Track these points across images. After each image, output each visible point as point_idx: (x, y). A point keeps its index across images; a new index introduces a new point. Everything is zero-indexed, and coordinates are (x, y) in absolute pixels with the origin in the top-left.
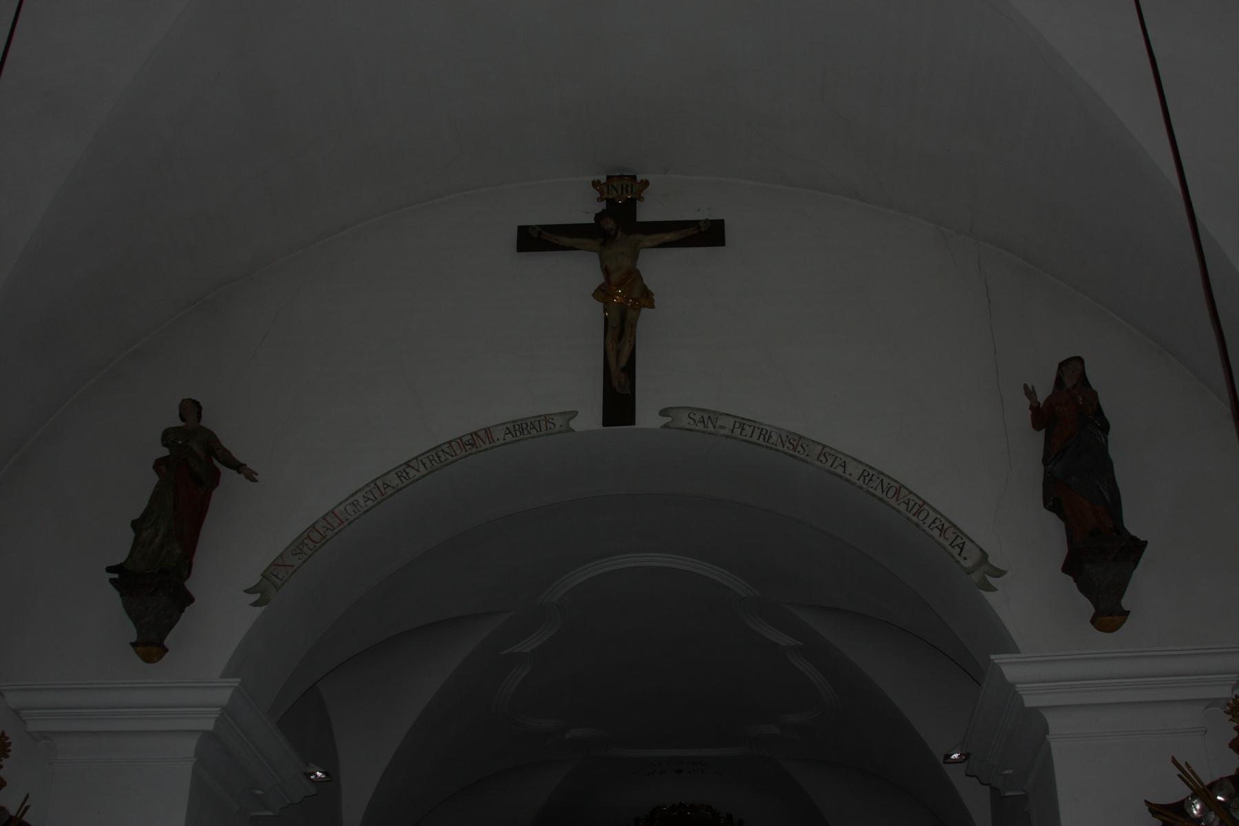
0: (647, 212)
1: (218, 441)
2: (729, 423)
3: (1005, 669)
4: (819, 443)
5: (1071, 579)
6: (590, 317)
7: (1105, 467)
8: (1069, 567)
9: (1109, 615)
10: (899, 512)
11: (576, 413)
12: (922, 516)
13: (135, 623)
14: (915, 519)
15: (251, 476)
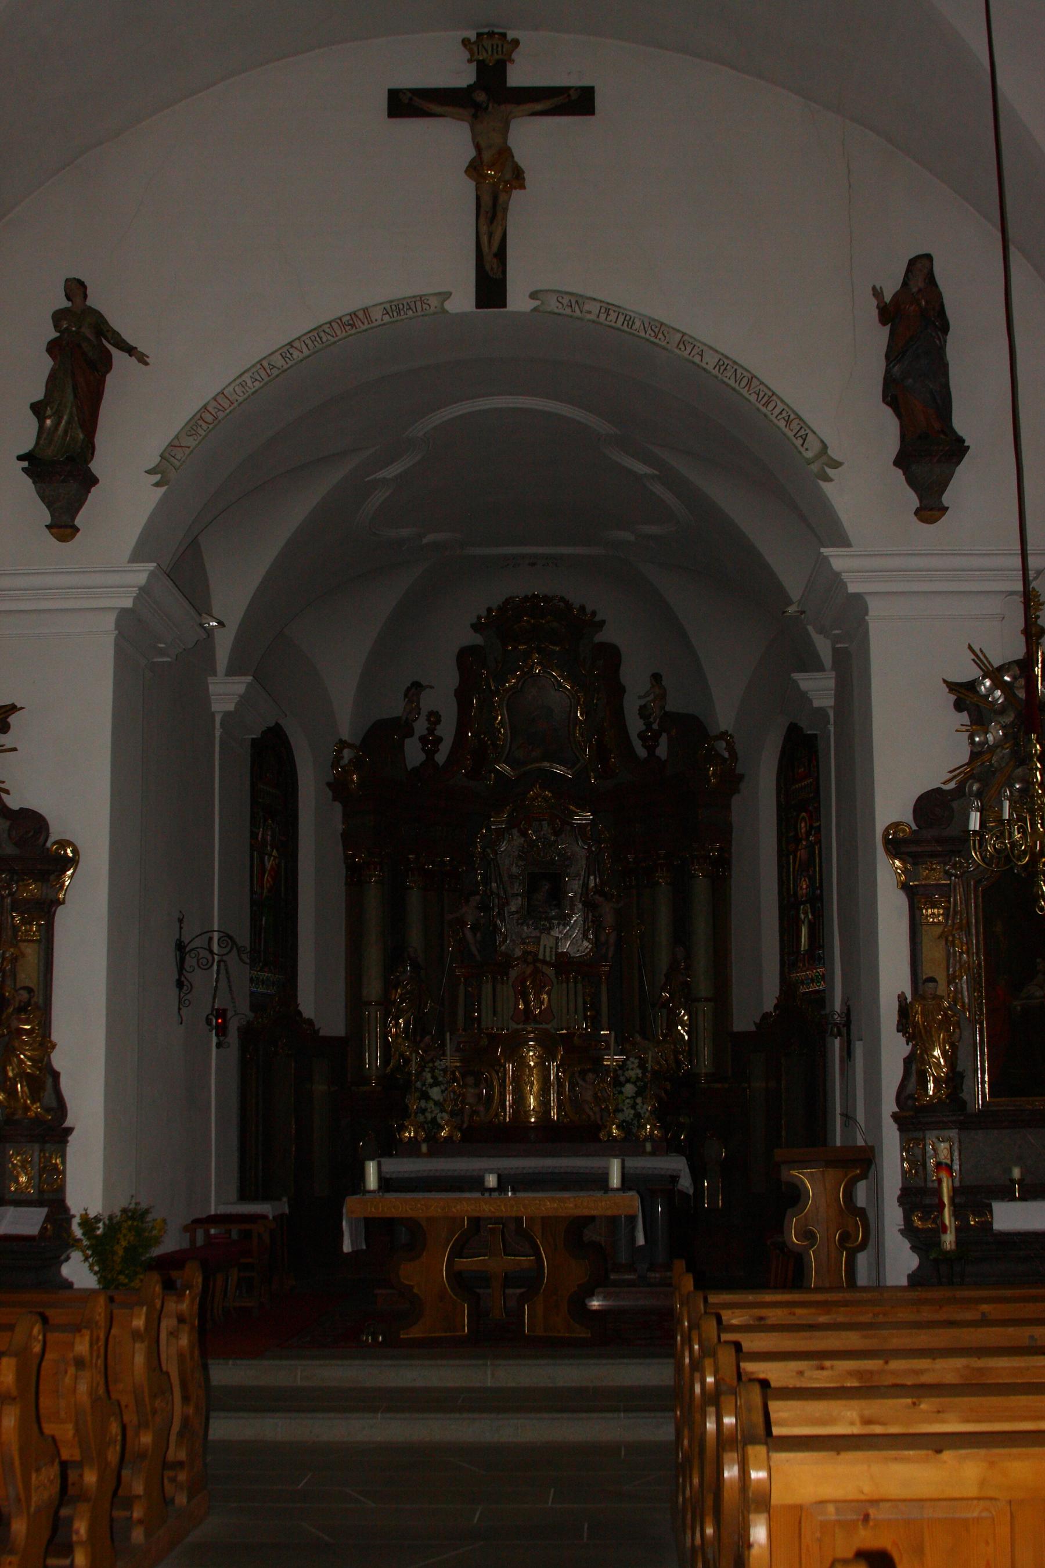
0: (518, 76)
1: (107, 322)
2: (594, 308)
3: (832, 561)
4: (678, 331)
5: (900, 472)
6: (461, 195)
7: (940, 367)
8: (899, 462)
9: (931, 510)
10: (749, 401)
11: (451, 294)
12: (771, 406)
13: (48, 507)
14: (764, 409)
15: (142, 359)
